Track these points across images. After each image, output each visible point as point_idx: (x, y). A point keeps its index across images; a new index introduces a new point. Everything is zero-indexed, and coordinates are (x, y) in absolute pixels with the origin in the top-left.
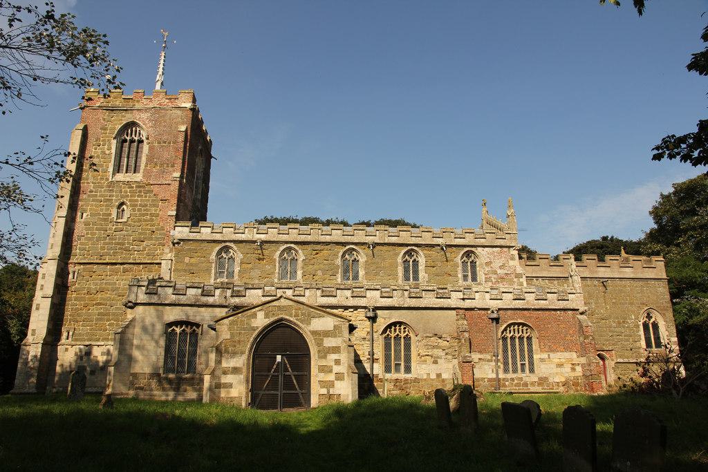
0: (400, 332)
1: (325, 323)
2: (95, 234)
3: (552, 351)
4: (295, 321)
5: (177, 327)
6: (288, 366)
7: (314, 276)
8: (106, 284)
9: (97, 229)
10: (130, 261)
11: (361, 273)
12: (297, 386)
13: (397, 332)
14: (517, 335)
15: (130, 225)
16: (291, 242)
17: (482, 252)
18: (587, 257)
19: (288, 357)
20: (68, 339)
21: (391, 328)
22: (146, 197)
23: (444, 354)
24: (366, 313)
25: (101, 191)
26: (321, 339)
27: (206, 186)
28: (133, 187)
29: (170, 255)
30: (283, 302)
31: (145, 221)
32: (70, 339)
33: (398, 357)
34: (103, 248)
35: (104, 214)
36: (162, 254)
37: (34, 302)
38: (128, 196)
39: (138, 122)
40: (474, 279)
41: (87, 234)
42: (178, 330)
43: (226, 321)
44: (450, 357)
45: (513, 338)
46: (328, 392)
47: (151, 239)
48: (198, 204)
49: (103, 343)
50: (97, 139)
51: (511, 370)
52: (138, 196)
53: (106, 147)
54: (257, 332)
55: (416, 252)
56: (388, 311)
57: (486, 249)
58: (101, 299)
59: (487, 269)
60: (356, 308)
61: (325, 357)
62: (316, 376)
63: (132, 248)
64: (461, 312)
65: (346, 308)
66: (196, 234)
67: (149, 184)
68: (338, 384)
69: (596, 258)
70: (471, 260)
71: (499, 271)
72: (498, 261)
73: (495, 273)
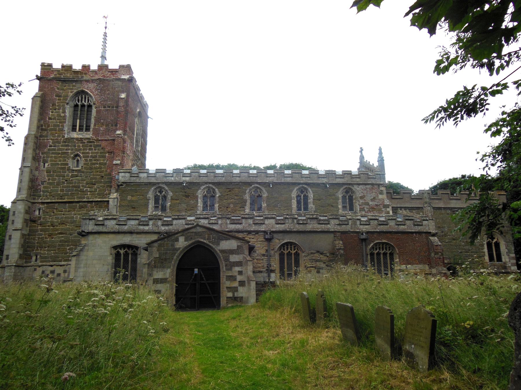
1: (232, 244)
2: (55, 179)
4: (208, 243)
5: (121, 249)
6: (203, 276)
7: (227, 208)
9: (56, 176)
12: (210, 292)
14: (382, 252)
15: (83, 172)
17: (358, 189)
18: (441, 192)
20: (36, 261)
21: (284, 247)
25: (58, 146)
26: (228, 256)
28: (84, 143)
29: (115, 194)
31: (96, 168)
32: (38, 261)
35: (62, 164)
36: (110, 194)
38: (81, 150)
39: (86, 90)
40: (351, 209)
42: (122, 252)
43: (156, 245)
45: (379, 254)
46: (234, 295)
47: (101, 182)
50: (54, 105)
52: (89, 149)
53: (61, 111)
54: (179, 252)
56: (389, 320)
57: (361, 186)
58: (62, 229)
59: (361, 201)
60: (257, 232)
61: (230, 269)
62: (225, 283)
63: (86, 190)
64: (338, 234)
65: (249, 232)
66: (136, 178)
67: (98, 140)
68: (241, 289)
71: (371, 203)
72: (370, 195)
73: (368, 204)
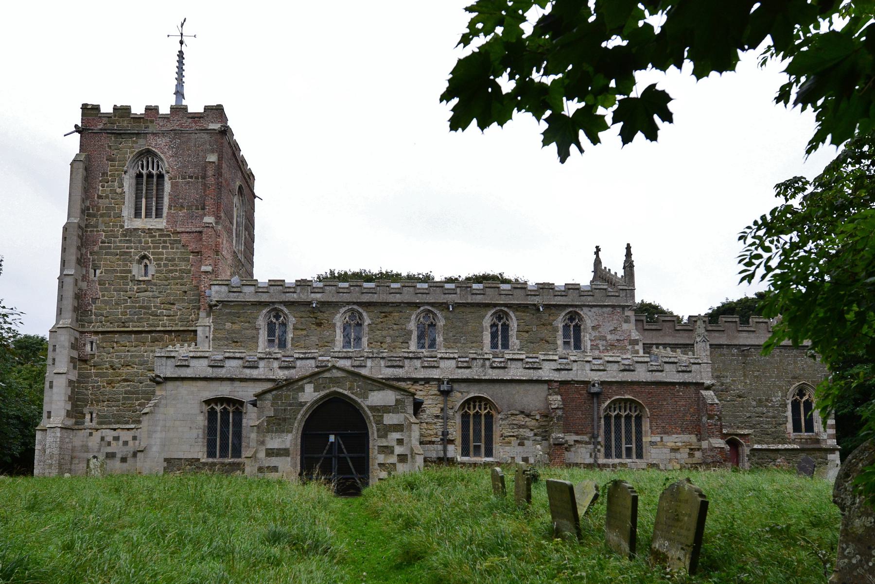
0: (480, 409)
3: (665, 433)
4: (350, 395)
5: (217, 406)
7: (381, 343)
8: (131, 356)
10: (158, 329)
11: (439, 339)
13: (477, 409)
14: (623, 414)
15: (155, 285)
16: (354, 303)
17: (589, 313)
18: (724, 319)
19: (342, 436)
21: (469, 404)
22: (172, 248)
23: (532, 435)
24: (439, 386)
25: (115, 242)
27: (249, 234)
28: (155, 236)
30: (336, 374)
31: (174, 278)
33: (477, 438)
34: (124, 313)
35: (122, 271)
37: (47, 379)
38: (149, 248)
39: (154, 149)
40: (577, 346)
41: (103, 296)
42: (218, 408)
43: (269, 396)
44: (539, 438)
45: (618, 417)
48: (241, 257)
49: (133, 426)
51: (614, 454)
52: (163, 247)
53: (116, 184)
54: (305, 408)
55: (507, 314)
59: (594, 334)
60: (427, 381)
61: (385, 436)
63: (160, 313)
65: (415, 381)
69: (737, 320)
70: (574, 324)
71: (609, 337)
73: (604, 338)
